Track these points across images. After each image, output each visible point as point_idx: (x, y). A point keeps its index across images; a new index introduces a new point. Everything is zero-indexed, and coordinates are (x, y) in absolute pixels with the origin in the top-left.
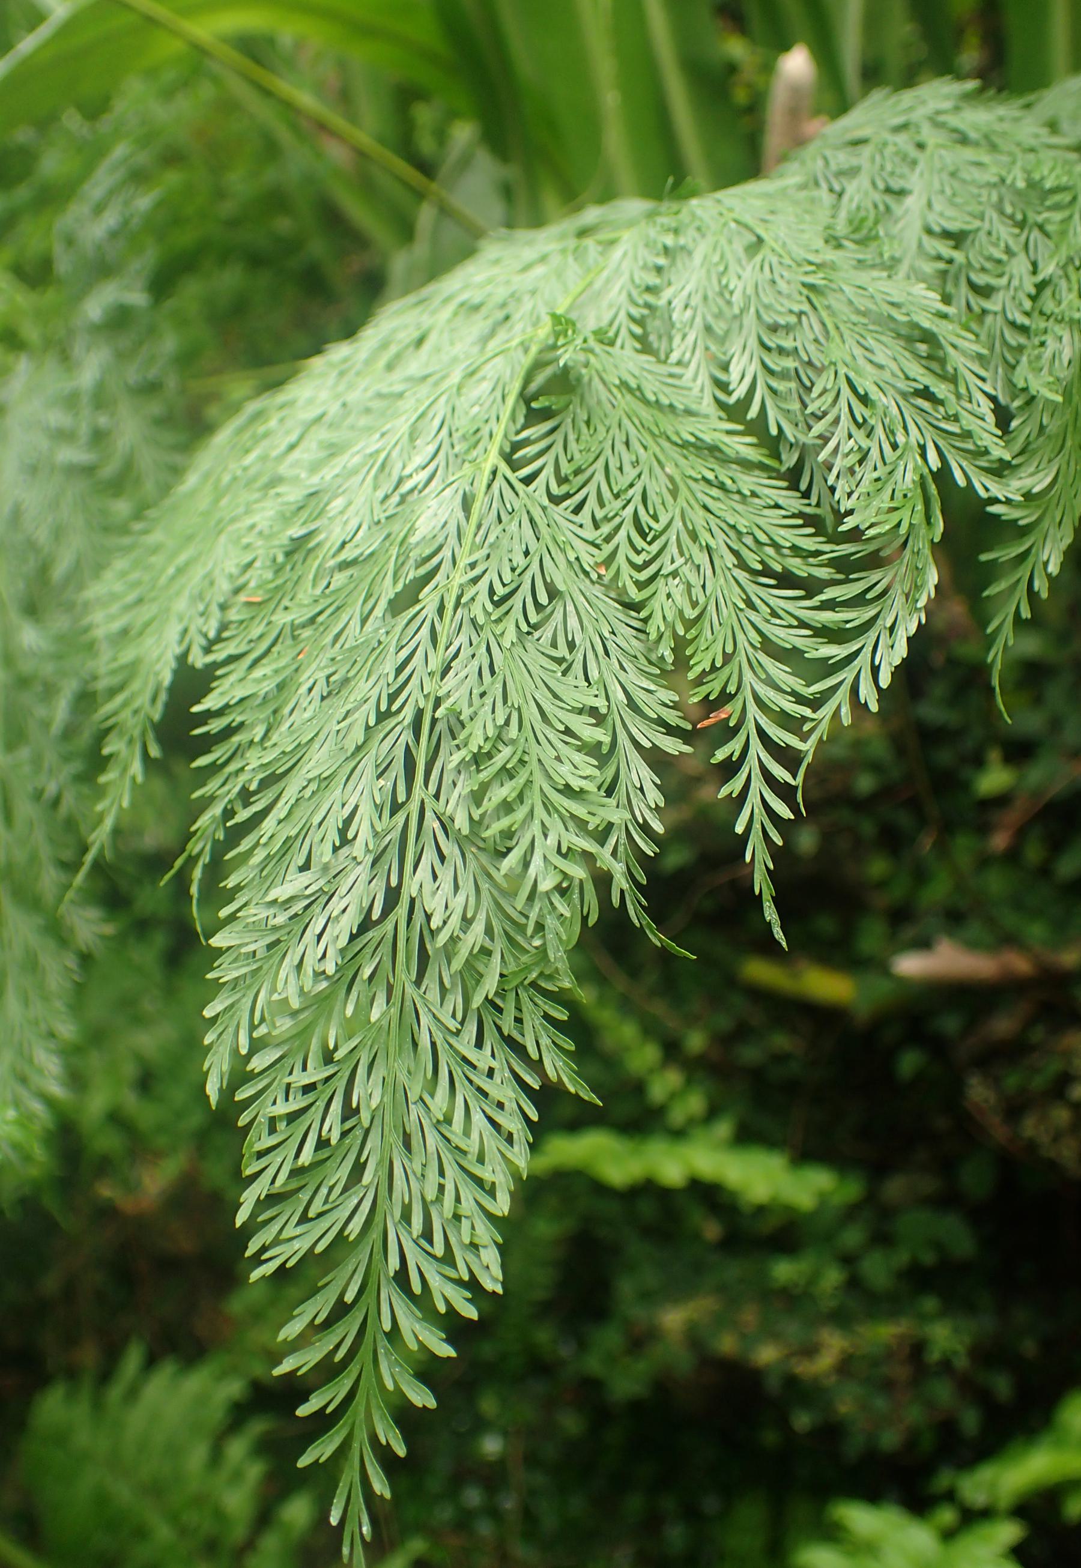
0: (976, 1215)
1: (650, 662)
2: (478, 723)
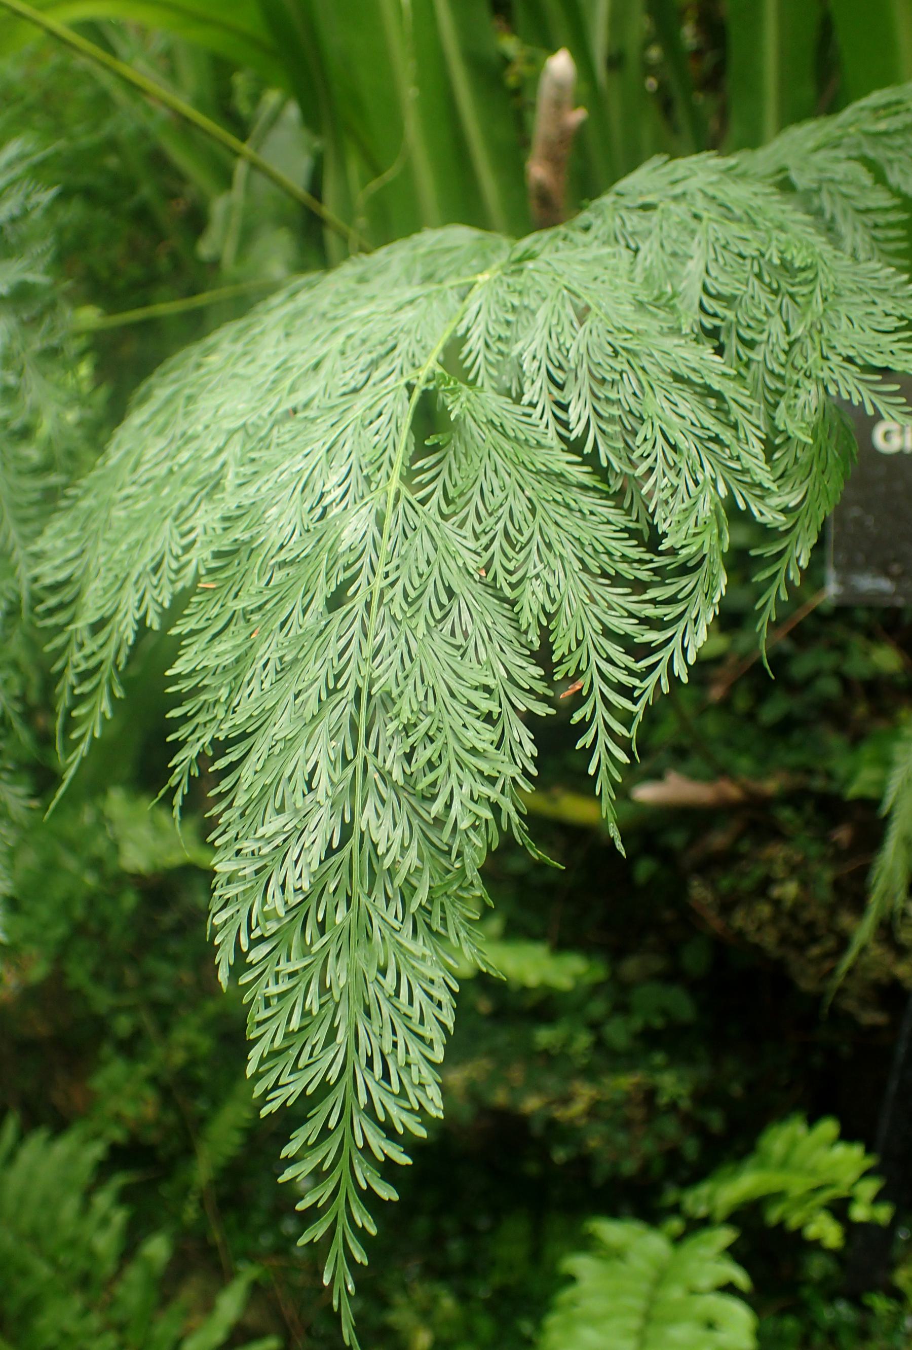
0: (694, 987)
1: (522, 645)
2: (405, 697)
